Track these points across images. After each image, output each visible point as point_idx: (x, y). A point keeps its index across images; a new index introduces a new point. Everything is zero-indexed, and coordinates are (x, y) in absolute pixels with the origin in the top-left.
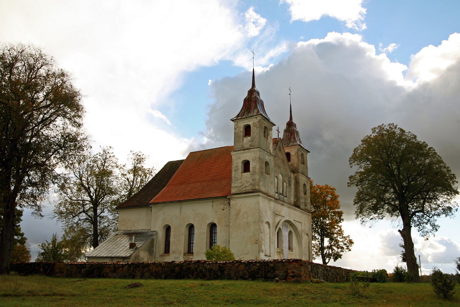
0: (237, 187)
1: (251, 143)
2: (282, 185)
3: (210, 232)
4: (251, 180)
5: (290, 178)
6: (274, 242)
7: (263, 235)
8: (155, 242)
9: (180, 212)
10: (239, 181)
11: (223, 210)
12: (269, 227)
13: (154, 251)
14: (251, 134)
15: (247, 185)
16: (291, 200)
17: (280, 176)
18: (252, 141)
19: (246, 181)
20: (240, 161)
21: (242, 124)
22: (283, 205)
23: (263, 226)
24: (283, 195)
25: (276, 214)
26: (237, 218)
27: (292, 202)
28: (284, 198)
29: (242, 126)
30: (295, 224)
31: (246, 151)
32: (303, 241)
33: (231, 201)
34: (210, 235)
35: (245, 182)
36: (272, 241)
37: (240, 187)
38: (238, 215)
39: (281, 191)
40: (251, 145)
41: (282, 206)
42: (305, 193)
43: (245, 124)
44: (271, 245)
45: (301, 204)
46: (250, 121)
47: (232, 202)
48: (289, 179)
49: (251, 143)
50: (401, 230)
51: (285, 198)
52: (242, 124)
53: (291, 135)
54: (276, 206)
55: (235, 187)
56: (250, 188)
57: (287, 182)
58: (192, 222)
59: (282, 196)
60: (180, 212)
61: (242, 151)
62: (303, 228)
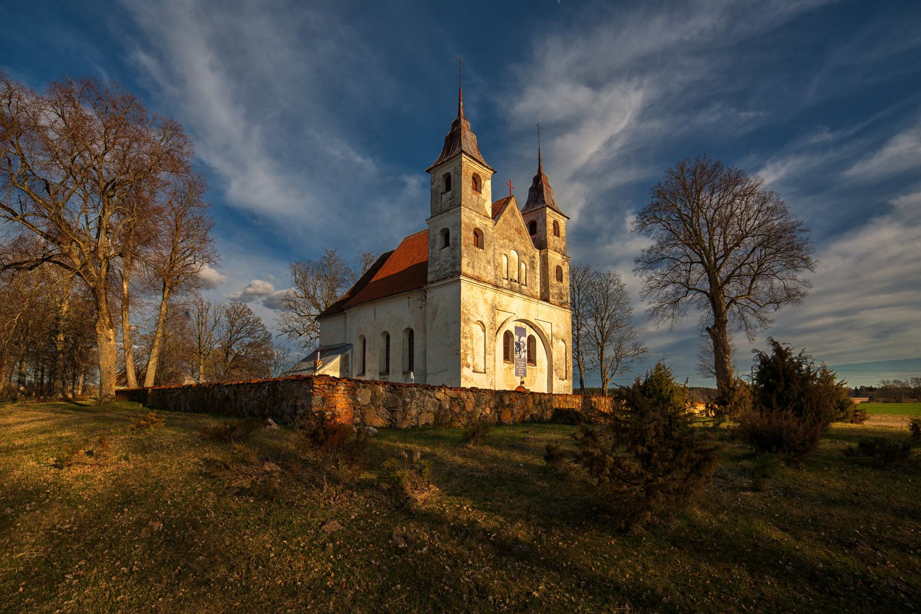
0: (434, 271)
1: (450, 201)
2: (517, 267)
3: (409, 340)
4: (450, 259)
5: (534, 257)
6: (492, 352)
7: (469, 341)
8: (350, 358)
9: (375, 314)
10: (437, 263)
11: (420, 308)
12: (484, 331)
13: (350, 370)
14: (452, 187)
15: (446, 266)
16: (536, 290)
17: (514, 254)
18: (453, 197)
19: (445, 261)
20: (438, 231)
21: (440, 173)
22: (511, 296)
23: (470, 327)
24: (519, 283)
25: (495, 309)
26: (434, 319)
27: (537, 292)
28: (520, 287)
29: (441, 177)
30: (537, 325)
31: (444, 214)
32: (554, 349)
33: (427, 293)
34: (409, 345)
35: (444, 263)
36: (488, 350)
37: (438, 271)
38: (435, 313)
39: (516, 277)
40: (451, 203)
41: (510, 298)
42: (560, 279)
43: (444, 173)
44: (487, 356)
45: (551, 296)
46: (450, 167)
47: (429, 295)
48: (530, 258)
49: (450, 201)
50: (710, 327)
51: (523, 287)
52: (440, 173)
53: (538, 195)
54: (497, 297)
55: (431, 272)
56: (450, 270)
57: (527, 263)
58: (386, 329)
59: (518, 284)
60: (375, 314)
61: (440, 216)
62: (553, 331)
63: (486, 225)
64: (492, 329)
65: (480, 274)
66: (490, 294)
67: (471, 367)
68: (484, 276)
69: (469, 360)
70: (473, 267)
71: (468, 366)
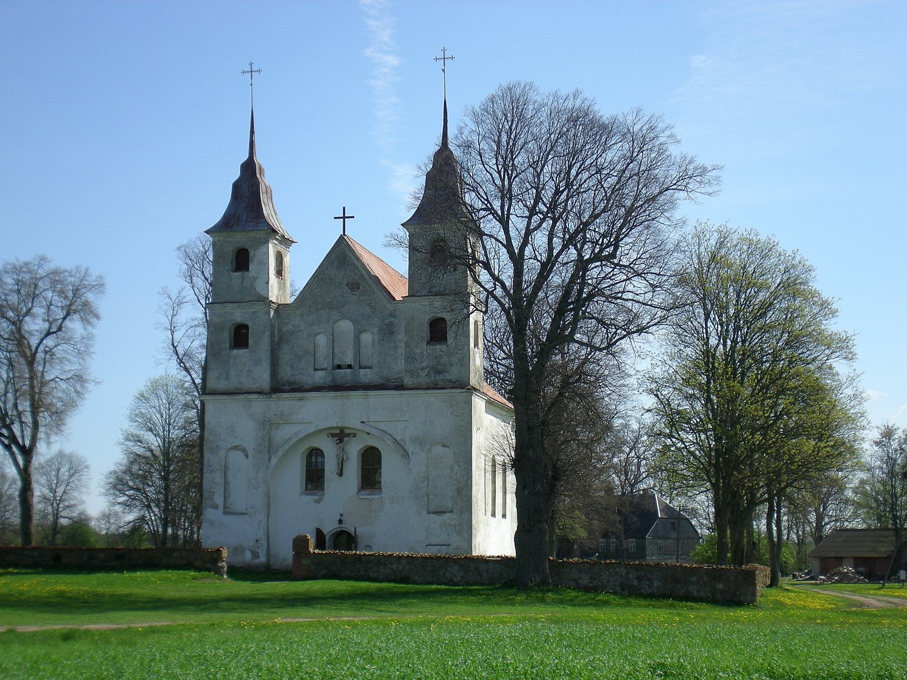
22: (300, 399)
63: (254, 313)
64: (260, 452)
65: (240, 383)
66: (259, 404)
67: (221, 509)
68: (249, 384)
69: (219, 499)
70: (227, 378)
71: (215, 507)
